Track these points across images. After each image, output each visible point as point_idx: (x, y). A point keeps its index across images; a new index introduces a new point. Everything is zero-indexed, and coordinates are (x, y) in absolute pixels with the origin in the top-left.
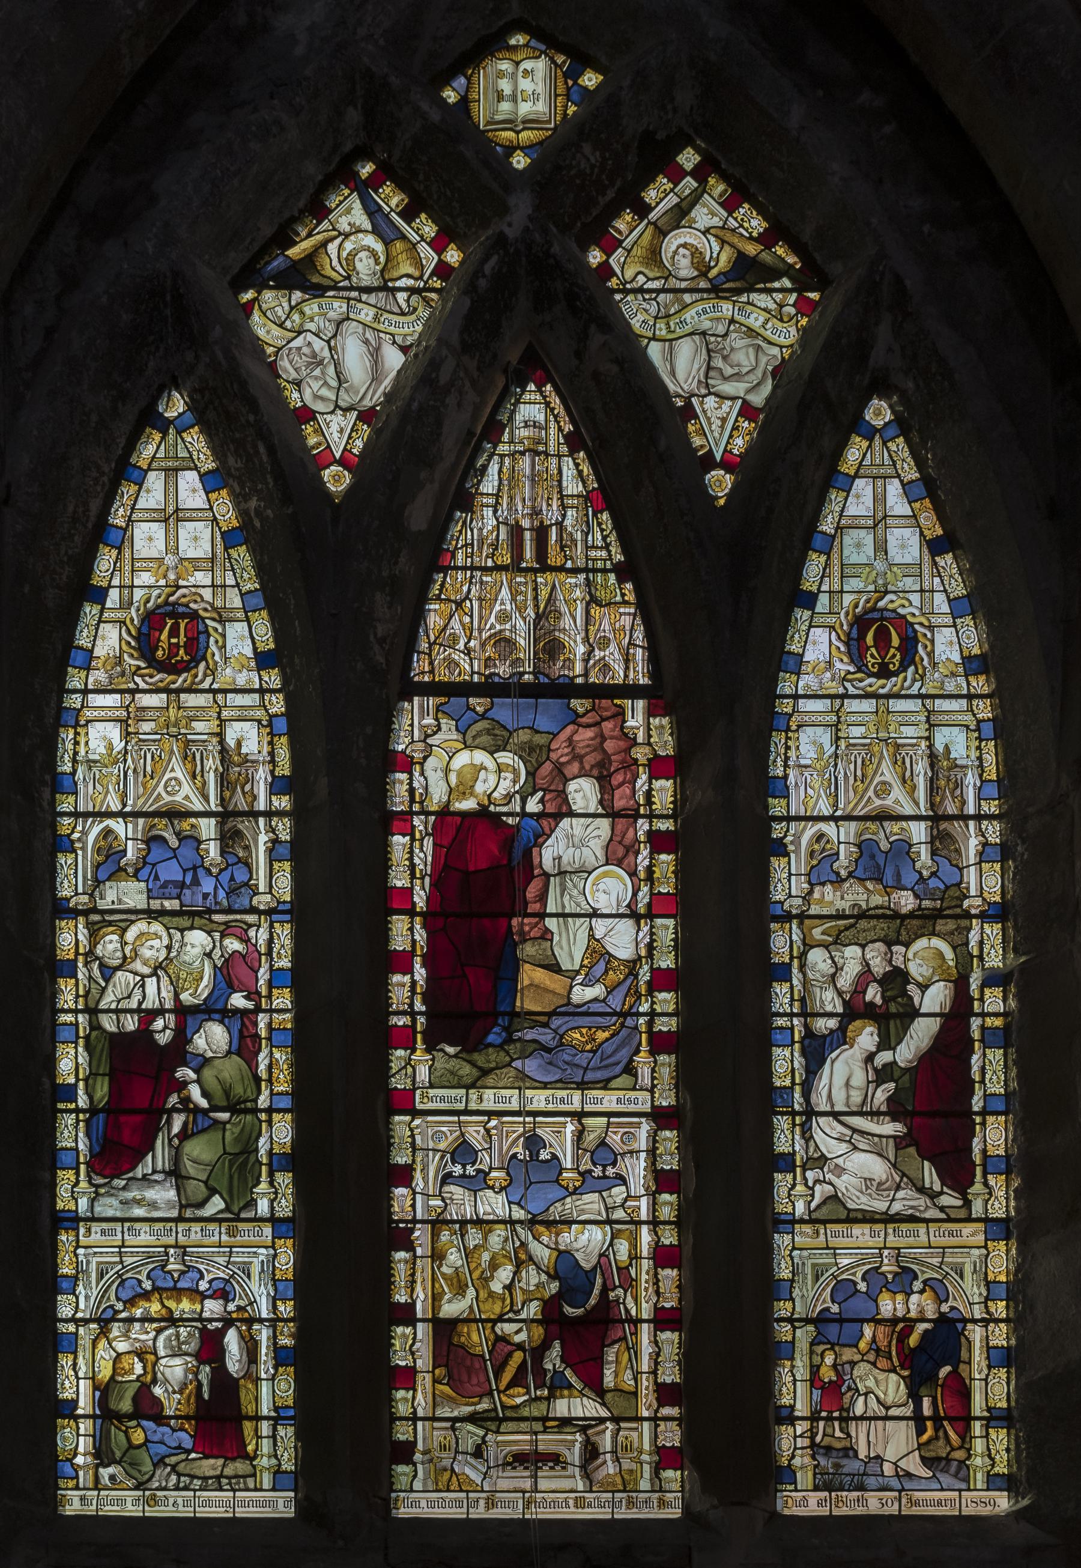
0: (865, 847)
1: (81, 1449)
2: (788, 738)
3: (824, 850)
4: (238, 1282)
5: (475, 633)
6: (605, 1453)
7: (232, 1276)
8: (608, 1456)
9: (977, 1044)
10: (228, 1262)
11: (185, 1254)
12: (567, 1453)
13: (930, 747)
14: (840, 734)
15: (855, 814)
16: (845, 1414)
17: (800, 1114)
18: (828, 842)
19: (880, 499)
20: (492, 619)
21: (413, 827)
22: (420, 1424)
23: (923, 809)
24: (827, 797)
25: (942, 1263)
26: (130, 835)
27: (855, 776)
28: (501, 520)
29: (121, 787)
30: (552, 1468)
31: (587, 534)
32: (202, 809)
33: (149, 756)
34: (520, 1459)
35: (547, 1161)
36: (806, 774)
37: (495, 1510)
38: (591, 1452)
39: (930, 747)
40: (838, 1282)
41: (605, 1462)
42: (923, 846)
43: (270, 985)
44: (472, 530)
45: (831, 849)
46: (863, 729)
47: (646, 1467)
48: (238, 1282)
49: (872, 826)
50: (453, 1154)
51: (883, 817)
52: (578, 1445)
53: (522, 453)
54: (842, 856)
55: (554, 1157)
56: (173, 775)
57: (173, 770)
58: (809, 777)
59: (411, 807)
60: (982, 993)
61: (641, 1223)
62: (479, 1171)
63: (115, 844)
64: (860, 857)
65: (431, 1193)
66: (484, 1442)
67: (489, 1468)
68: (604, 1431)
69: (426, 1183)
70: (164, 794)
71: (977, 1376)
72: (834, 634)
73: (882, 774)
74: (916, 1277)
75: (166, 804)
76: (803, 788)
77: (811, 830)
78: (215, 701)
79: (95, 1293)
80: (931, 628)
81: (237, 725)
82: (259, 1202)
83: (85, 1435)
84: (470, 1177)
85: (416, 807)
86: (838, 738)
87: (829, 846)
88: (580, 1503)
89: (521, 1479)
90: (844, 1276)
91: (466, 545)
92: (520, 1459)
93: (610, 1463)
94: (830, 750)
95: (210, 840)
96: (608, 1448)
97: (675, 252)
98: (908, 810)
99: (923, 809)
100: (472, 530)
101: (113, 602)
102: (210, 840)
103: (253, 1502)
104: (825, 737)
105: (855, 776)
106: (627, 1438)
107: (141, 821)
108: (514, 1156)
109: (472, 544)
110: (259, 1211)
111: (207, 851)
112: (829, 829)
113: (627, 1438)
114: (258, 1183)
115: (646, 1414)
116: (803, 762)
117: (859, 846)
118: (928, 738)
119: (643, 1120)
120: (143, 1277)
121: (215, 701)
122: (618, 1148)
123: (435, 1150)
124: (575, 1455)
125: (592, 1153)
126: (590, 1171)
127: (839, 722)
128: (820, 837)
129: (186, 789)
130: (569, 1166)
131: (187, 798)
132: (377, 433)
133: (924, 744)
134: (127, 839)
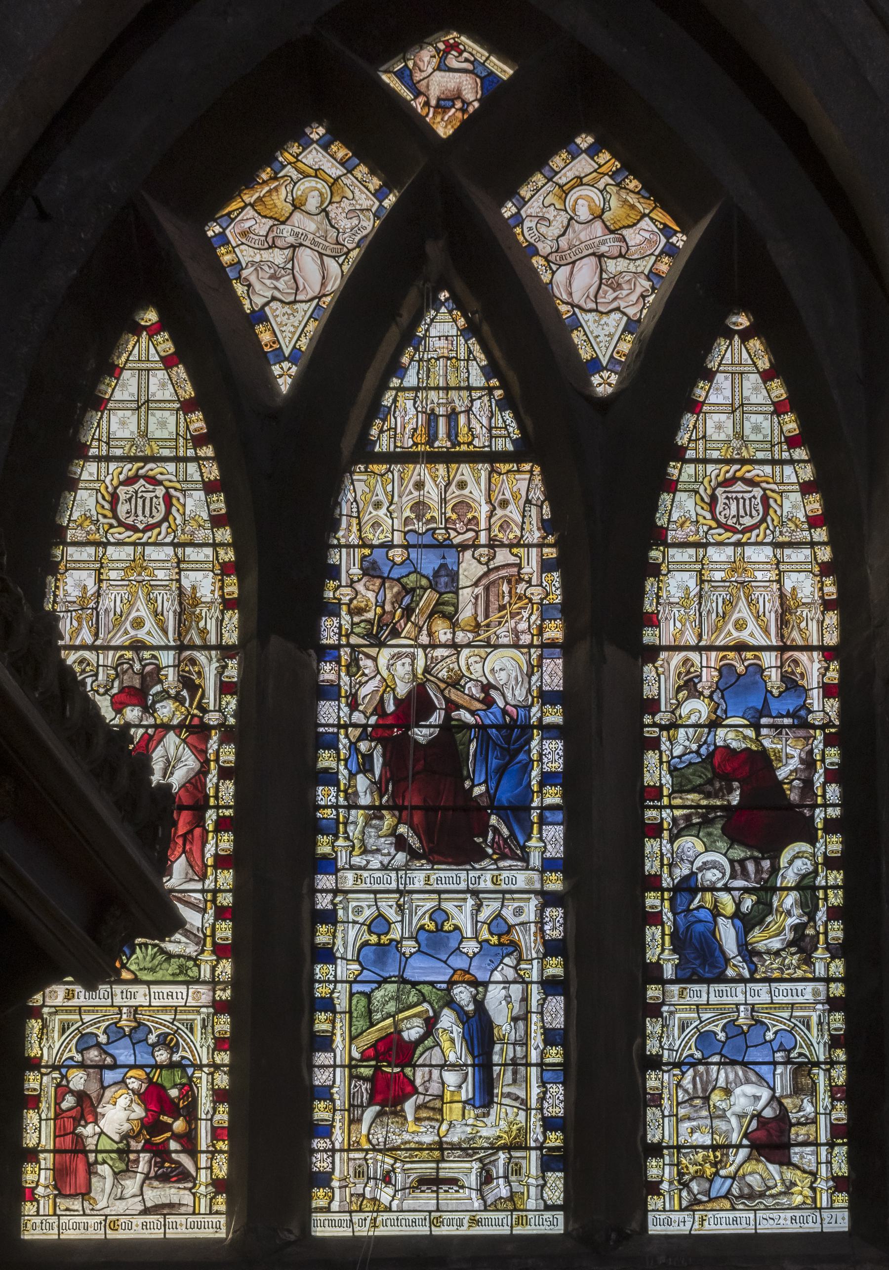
0: (725, 670)
1: (42, 1181)
2: (57, 580)
4: (182, 1037)
5: (396, 499)
6: (498, 1178)
7: (176, 1032)
8: (501, 1181)
10: (791, 1016)
11: (753, 1010)
12: (464, 1179)
13: (180, 588)
14: (103, 577)
15: (717, 644)
16: (719, 1140)
17: (668, 890)
18: (693, 665)
19: (143, 386)
20: (410, 486)
21: (340, 657)
22: (337, 1156)
23: (171, 639)
24: (693, 629)
25: (174, 1019)
26: (704, 664)
28: (420, 409)
30: (457, 1191)
31: (491, 418)
32: (764, 644)
34: (424, 1182)
35: (450, 932)
37: (528, 1227)
38: (487, 1178)
39: (180, 588)
40: (83, 1035)
41: (498, 1186)
42: (774, 670)
43: (542, 784)
44: (395, 418)
46: (722, 574)
47: (533, 1190)
48: (182, 1037)
49: (731, 655)
50: (369, 926)
51: (741, 647)
52: (474, 1171)
53: (438, 359)
55: (457, 928)
56: (740, 615)
57: (138, 610)
59: (339, 640)
60: (824, 791)
61: (532, 982)
62: (391, 940)
63: (692, 670)
65: (350, 957)
66: (394, 1170)
67: (396, 1191)
68: (497, 1160)
69: (346, 948)
71: (822, 1111)
72: (99, 494)
73: (138, 610)
74: (150, 1032)
75: (734, 639)
76: (672, 621)
77: (677, 658)
78: (176, 555)
79: (57, 1045)
80: (781, 494)
81: (794, 576)
82: (817, 965)
83: (46, 1169)
84: (384, 945)
85: (344, 641)
86: (100, 581)
88: (474, 1221)
89: (426, 1200)
90: (88, 1030)
91: (389, 430)
92: (424, 1182)
93: (502, 1187)
94: (694, 591)
95: (168, 666)
96: (501, 1173)
97: (576, 202)
98: (762, 641)
99: (171, 639)
100: (395, 418)
101: (91, 474)
102: (168, 666)
103: (77, 1226)
104: (691, 582)
106: (516, 1165)
108: (422, 928)
109: (395, 429)
111: (166, 676)
112: (694, 656)
113: (516, 1165)
114: (816, 949)
115: (533, 1144)
116: (672, 600)
117: (720, 671)
118: (778, 581)
119: (469, 896)
120: (99, 1032)
121: (176, 555)
122: (512, 920)
123: (355, 922)
124: (472, 1180)
125: (489, 925)
126: (487, 941)
127: (102, 567)
128: (686, 661)
129: (752, 626)
130: (469, 935)
131: (752, 635)
132: (639, 341)
133: (775, 586)
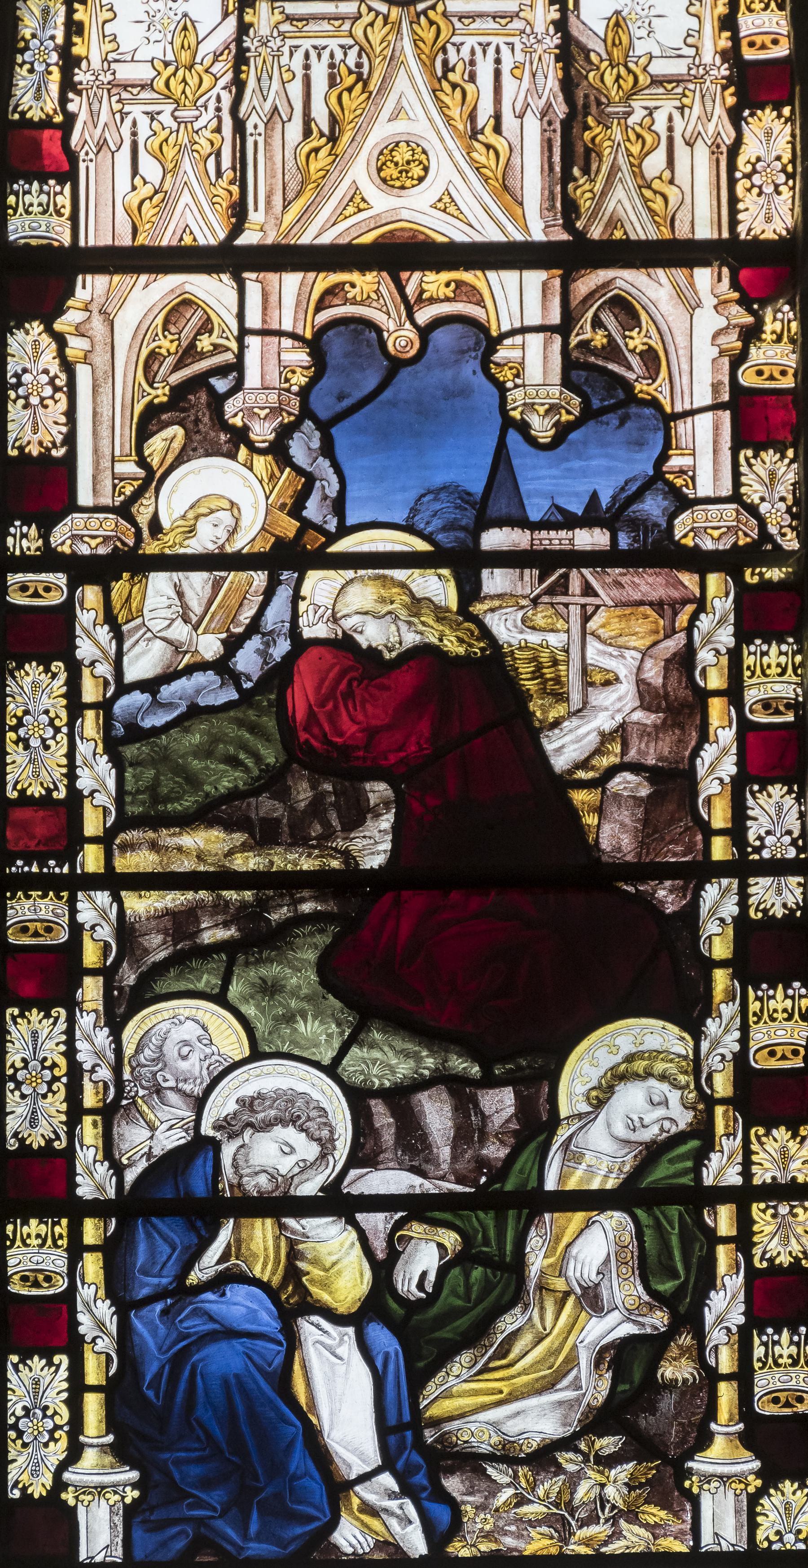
3: (190, 353)
9: (721, 978)
18: (206, 327)
27: (307, 120)
29: (226, 163)
32: (494, 235)
33: (320, 73)
36: (136, 111)
45: (217, 349)
54: (252, 378)
56: (400, 127)
58: (144, 123)
63: (205, 343)
64: (314, 381)
70: (371, 191)
76: (124, 157)
87: (205, 343)
95: (524, 330)
102: (524, 330)
105: (307, 120)
107: (292, 281)
110: (707, 1538)
114: (705, 1440)
134: (243, 332)
